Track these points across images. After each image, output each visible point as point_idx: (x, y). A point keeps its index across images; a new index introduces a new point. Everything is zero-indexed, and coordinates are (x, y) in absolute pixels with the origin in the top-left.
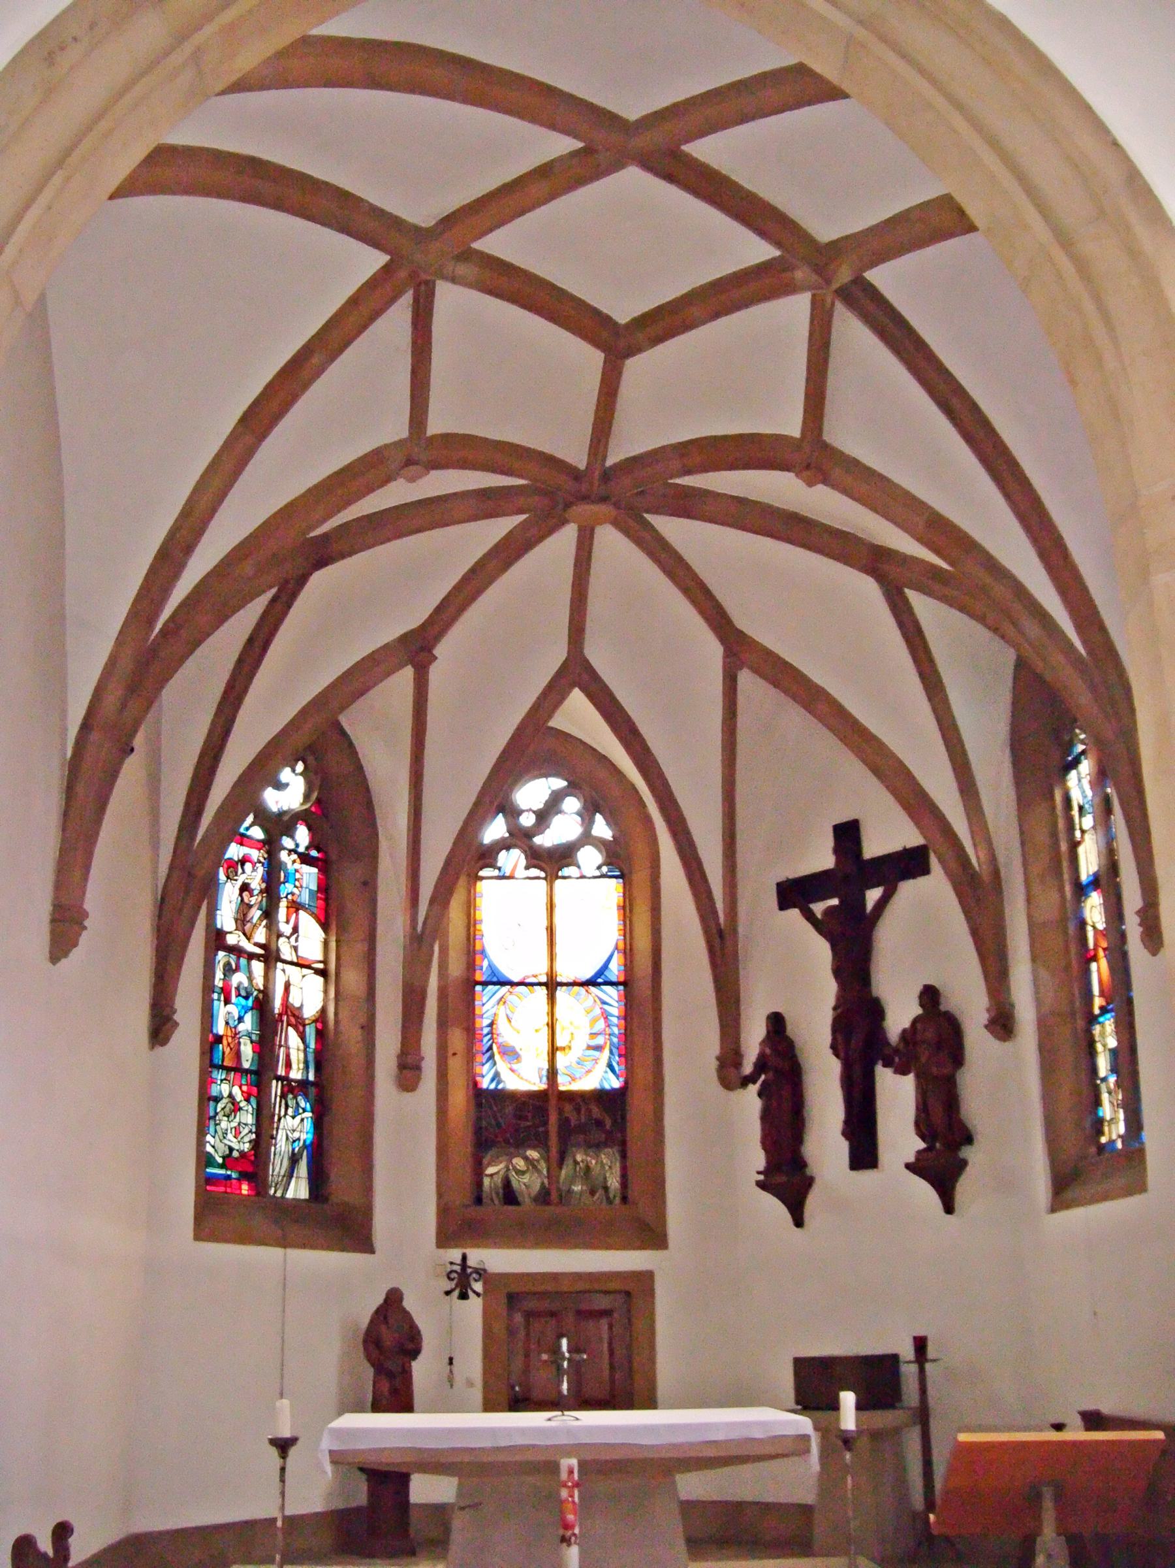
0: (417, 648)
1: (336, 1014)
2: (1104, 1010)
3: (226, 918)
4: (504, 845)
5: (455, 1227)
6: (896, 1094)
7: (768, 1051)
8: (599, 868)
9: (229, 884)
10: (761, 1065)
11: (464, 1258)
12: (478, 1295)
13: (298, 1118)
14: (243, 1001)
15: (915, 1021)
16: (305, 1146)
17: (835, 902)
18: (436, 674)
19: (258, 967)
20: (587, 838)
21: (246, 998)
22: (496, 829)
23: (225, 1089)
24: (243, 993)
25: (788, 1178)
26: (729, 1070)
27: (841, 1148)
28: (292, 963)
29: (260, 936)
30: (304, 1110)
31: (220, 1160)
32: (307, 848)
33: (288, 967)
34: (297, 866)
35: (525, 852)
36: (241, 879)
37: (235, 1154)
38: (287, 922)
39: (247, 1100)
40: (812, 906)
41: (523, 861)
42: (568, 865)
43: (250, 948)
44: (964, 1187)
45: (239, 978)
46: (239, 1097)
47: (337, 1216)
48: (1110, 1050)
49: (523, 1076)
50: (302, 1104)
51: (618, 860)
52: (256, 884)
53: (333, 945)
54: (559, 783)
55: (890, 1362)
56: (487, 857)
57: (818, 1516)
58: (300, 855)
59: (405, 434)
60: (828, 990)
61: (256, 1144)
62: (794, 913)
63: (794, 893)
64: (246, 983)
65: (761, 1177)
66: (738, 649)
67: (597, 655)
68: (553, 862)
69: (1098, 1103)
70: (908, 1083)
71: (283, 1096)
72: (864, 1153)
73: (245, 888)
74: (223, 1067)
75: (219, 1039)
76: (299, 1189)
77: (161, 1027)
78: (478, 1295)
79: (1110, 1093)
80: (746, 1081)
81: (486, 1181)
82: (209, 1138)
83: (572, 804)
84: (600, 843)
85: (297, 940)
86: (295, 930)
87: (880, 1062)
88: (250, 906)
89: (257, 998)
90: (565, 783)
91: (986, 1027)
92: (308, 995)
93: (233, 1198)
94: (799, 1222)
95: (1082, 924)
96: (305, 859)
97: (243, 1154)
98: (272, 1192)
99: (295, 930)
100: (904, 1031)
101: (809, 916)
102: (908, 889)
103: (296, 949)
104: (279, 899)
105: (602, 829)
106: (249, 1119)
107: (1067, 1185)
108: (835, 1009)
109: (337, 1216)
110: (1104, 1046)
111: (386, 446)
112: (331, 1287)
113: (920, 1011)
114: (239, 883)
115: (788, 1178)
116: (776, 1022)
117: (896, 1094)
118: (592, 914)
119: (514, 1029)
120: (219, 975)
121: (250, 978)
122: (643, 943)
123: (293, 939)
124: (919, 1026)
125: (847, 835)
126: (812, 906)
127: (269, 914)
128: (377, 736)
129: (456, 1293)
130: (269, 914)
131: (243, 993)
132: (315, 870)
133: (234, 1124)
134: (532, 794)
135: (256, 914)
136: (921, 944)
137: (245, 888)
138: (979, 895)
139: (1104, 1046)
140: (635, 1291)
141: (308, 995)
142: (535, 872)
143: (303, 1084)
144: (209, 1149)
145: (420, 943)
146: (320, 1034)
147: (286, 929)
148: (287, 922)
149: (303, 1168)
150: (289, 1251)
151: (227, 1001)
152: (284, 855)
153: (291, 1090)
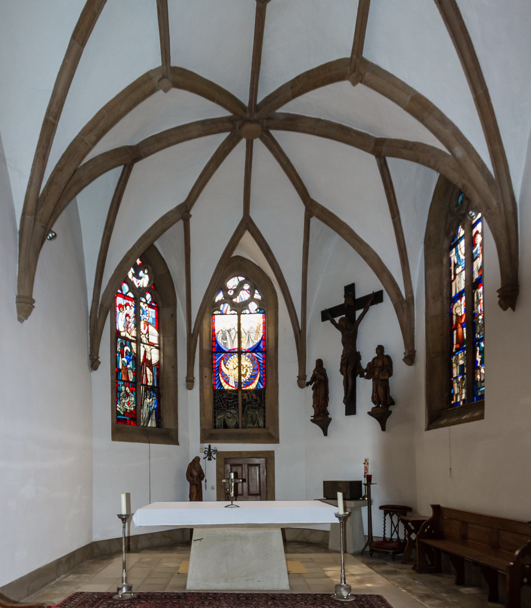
0: (183, 212)
1: (163, 362)
2: (458, 350)
3: (120, 326)
4: (221, 302)
5: (206, 436)
6: (365, 388)
7: (316, 373)
8: (256, 310)
9: (121, 313)
10: (314, 378)
11: (210, 446)
12: (215, 459)
13: (151, 399)
14: (129, 357)
15: (374, 359)
16: (154, 409)
17: (344, 316)
18: (193, 222)
19: (134, 345)
20: (252, 299)
21: (130, 356)
22: (220, 297)
23: (123, 388)
24: (128, 354)
25: (322, 419)
26: (302, 382)
27: (342, 407)
28: (146, 344)
29: (134, 333)
30: (153, 396)
31: (122, 413)
32: (150, 302)
33: (145, 346)
34: (147, 308)
35: (230, 304)
36: (126, 312)
37: (128, 411)
38: (145, 329)
39: (132, 392)
40: (335, 319)
41: (229, 308)
42: (245, 309)
43: (130, 338)
44: (389, 421)
45: (126, 348)
46: (128, 391)
47: (166, 433)
48: (460, 366)
49: (230, 386)
50: (152, 394)
51: (262, 309)
52: (132, 314)
53: (162, 338)
54: (241, 279)
55: (359, 484)
56: (216, 306)
57: (331, 533)
58: (148, 305)
59: (160, 64)
60: (340, 349)
61: (135, 408)
62: (328, 322)
63: (327, 315)
64: (129, 350)
65: (313, 418)
66: (313, 210)
67: (254, 215)
68: (240, 309)
69: (452, 387)
70: (370, 383)
71: (145, 391)
72: (351, 408)
73: (127, 315)
74: (121, 380)
75: (120, 370)
76: (152, 424)
77: (94, 364)
78: (215, 459)
79: (458, 383)
80: (308, 384)
81: (217, 421)
82: (118, 405)
83: (246, 287)
84: (256, 301)
85: (148, 336)
86: (148, 332)
87: (359, 375)
88: (129, 322)
89: (134, 356)
90: (244, 279)
91: (403, 360)
92: (154, 356)
93: (125, 426)
94: (325, 434)
95: (451, 314)
96: (150, 306)
97: (131, 411)
98: (142, 424)
99: (148, 332)
100: (369, 363)
101: (333, 322)
102: (373, 309)
103: (148, 339)
104: (141, 320)
105: (257, 296)
106: (133, 399)
107: (435, 420)
108: (342, 356)
109: (166, 433)
110: (457, 364)
111: (151, 71)
112: (164, 460)
113: (376, 355)
114: (125, 314)
115: (322, 419)
116: (320, 363)
117: (365, 388)
118: (253, 323)
119: (227, 368)
120: (119, 347)
121: (131, 348)
122: (271, 337)
123: (147, 335)
124: (376, 361)
125: (350, 289)
126: (335, 319)
127: (137, 325)
128: (169, 248)
129: (207, 458)
130: (137, 325)
131: (128, 354)
132: (154, 311)
133: (127, 401)
134: (232, 283)
135: (132, 325)
136: (381, 330)
137: (127, 315)
138: (404, 308)
139: (457, 364)
140: (269, 457)
141: (154, 356)
142: (233, 312)
143: (152, 388)
144: (118, 409)
145: (191, 338)
146: (158, 370)
147: (144, 332)
148: (145, 329)
149: (154, 417)
150: (151, 445)
151: (123, 357)
152: (141, 304)
153: (148, 389)
